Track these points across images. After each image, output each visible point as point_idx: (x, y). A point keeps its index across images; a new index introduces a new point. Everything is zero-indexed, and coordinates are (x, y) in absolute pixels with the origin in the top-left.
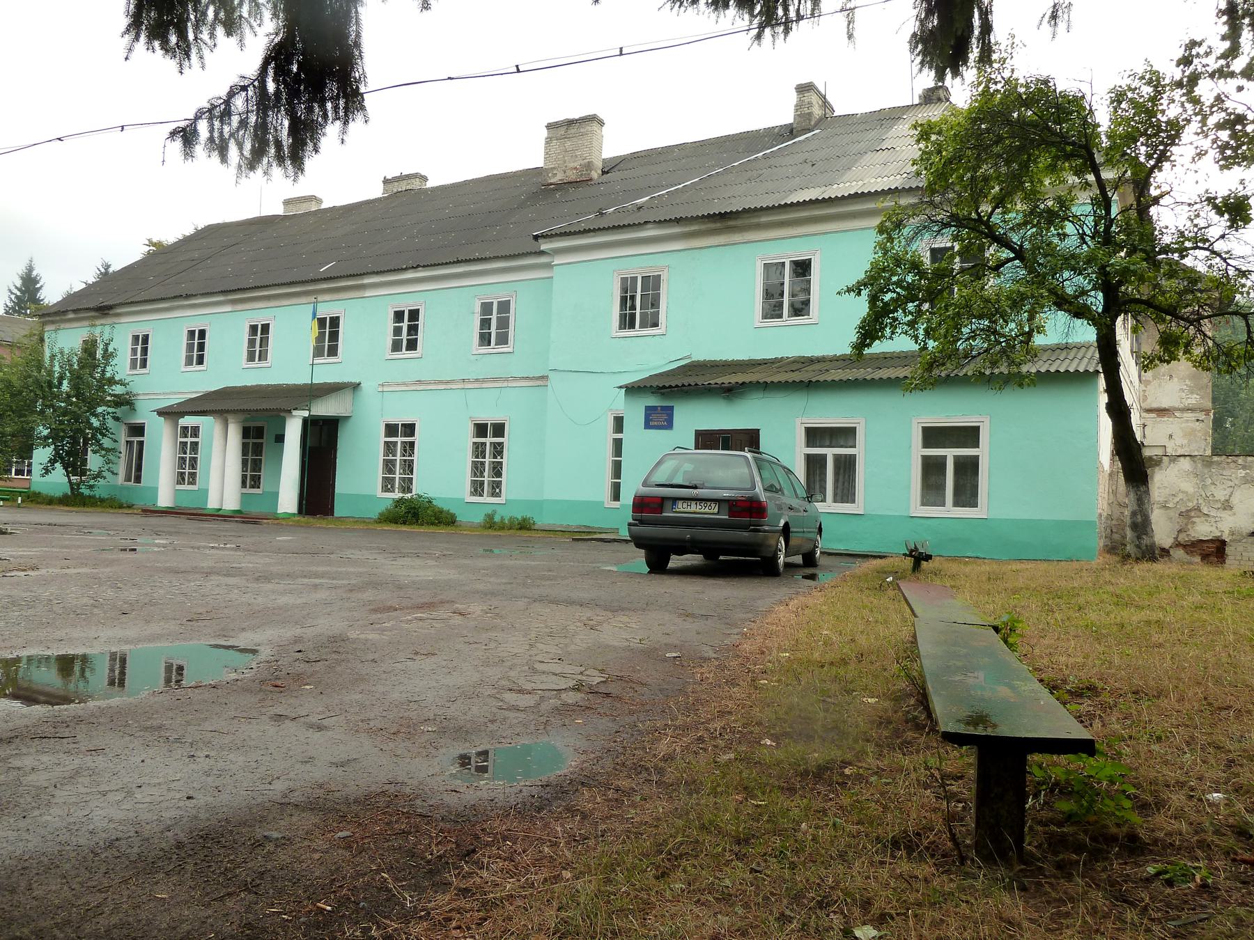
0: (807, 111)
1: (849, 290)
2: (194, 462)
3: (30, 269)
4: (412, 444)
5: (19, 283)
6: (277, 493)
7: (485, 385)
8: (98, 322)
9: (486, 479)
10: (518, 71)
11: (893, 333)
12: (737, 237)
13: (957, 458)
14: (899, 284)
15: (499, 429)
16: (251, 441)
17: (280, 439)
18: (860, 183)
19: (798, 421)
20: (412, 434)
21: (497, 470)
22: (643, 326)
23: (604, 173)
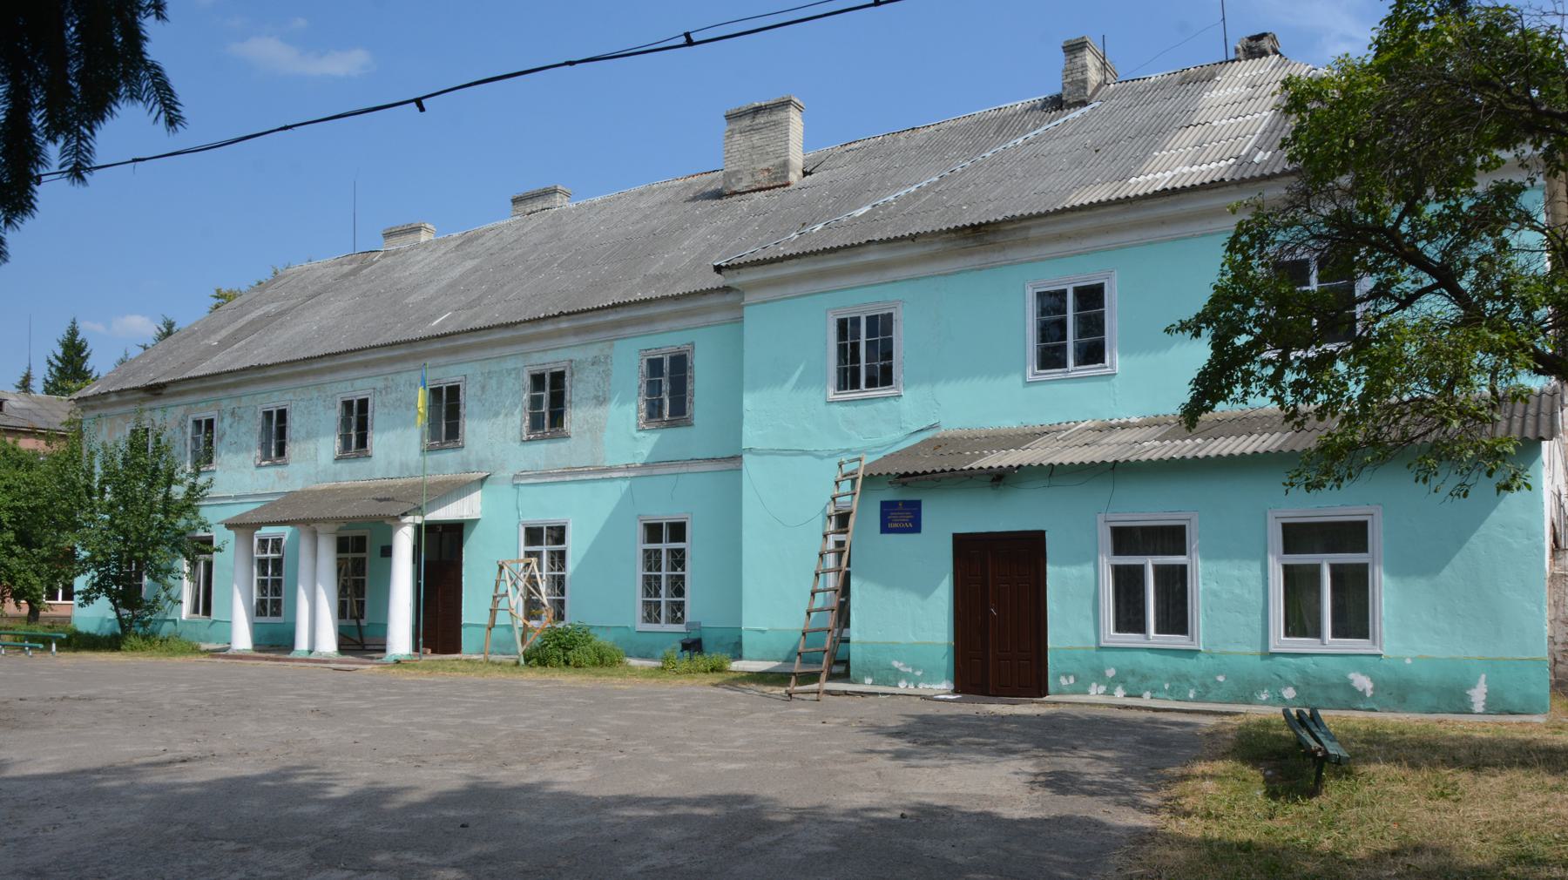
0: (1080, 77)
1: (1183, 327)
2: (277, 585)
3: (73, 333)
5: (60, 353)
7: (656, 471)
8: (147, 405)
9: (663, 599)
10: (418, 102)
11: (1246, 393)
12: (996, 257)
14: (1258, 320)
15: (678, 531)
16: (350, 555)
17: (387, 552)
18: (1168, 174)
19: (1100, 519)
21: (678, 587)
22: (871, 383)
23: (805, 174)
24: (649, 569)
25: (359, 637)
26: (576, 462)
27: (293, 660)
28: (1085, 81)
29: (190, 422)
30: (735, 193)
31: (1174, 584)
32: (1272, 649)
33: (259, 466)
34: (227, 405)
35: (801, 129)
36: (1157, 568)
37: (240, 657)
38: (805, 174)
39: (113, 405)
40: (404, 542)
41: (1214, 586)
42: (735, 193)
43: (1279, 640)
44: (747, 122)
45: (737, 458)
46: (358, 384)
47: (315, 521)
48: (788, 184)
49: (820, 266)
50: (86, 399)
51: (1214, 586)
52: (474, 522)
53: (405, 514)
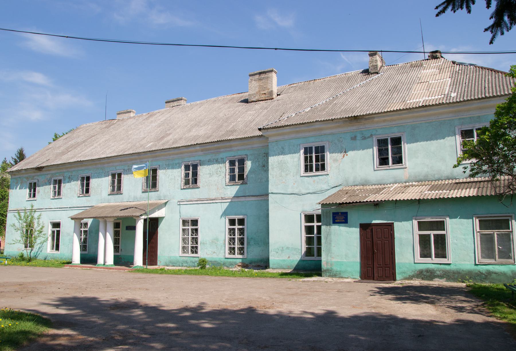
4: (196, 230)
6: (321, 260)
13: (434, 235)
20: (243, 225)
22: (317, 170)
23: (278, 95)
24: (231, 235)
25: (123, 260)
26: (202, 197)
27: (97, 268)
28: (377, 65)
29: (52, 180)
30: (253, 101)
31: (441, 241)
32: (416, 262)
33: (79, 197)
34: (67, 174)
35: (276, 80)
36: (434, 235)
37: (77, 266)
38: (278, 95)
39: (23, 174)
40: (140, 226)
41: (455, 241)
42: (253, 101)
43: (418, 259)
44: (257, 77)
45: (267, 195)
46: (118, 168)
47: (106, 217)
48: (273, 99)
49: (297, 129)
50: (12, 172)
51: (455, 241)
52: (162, 218)
53: (141, 215)
